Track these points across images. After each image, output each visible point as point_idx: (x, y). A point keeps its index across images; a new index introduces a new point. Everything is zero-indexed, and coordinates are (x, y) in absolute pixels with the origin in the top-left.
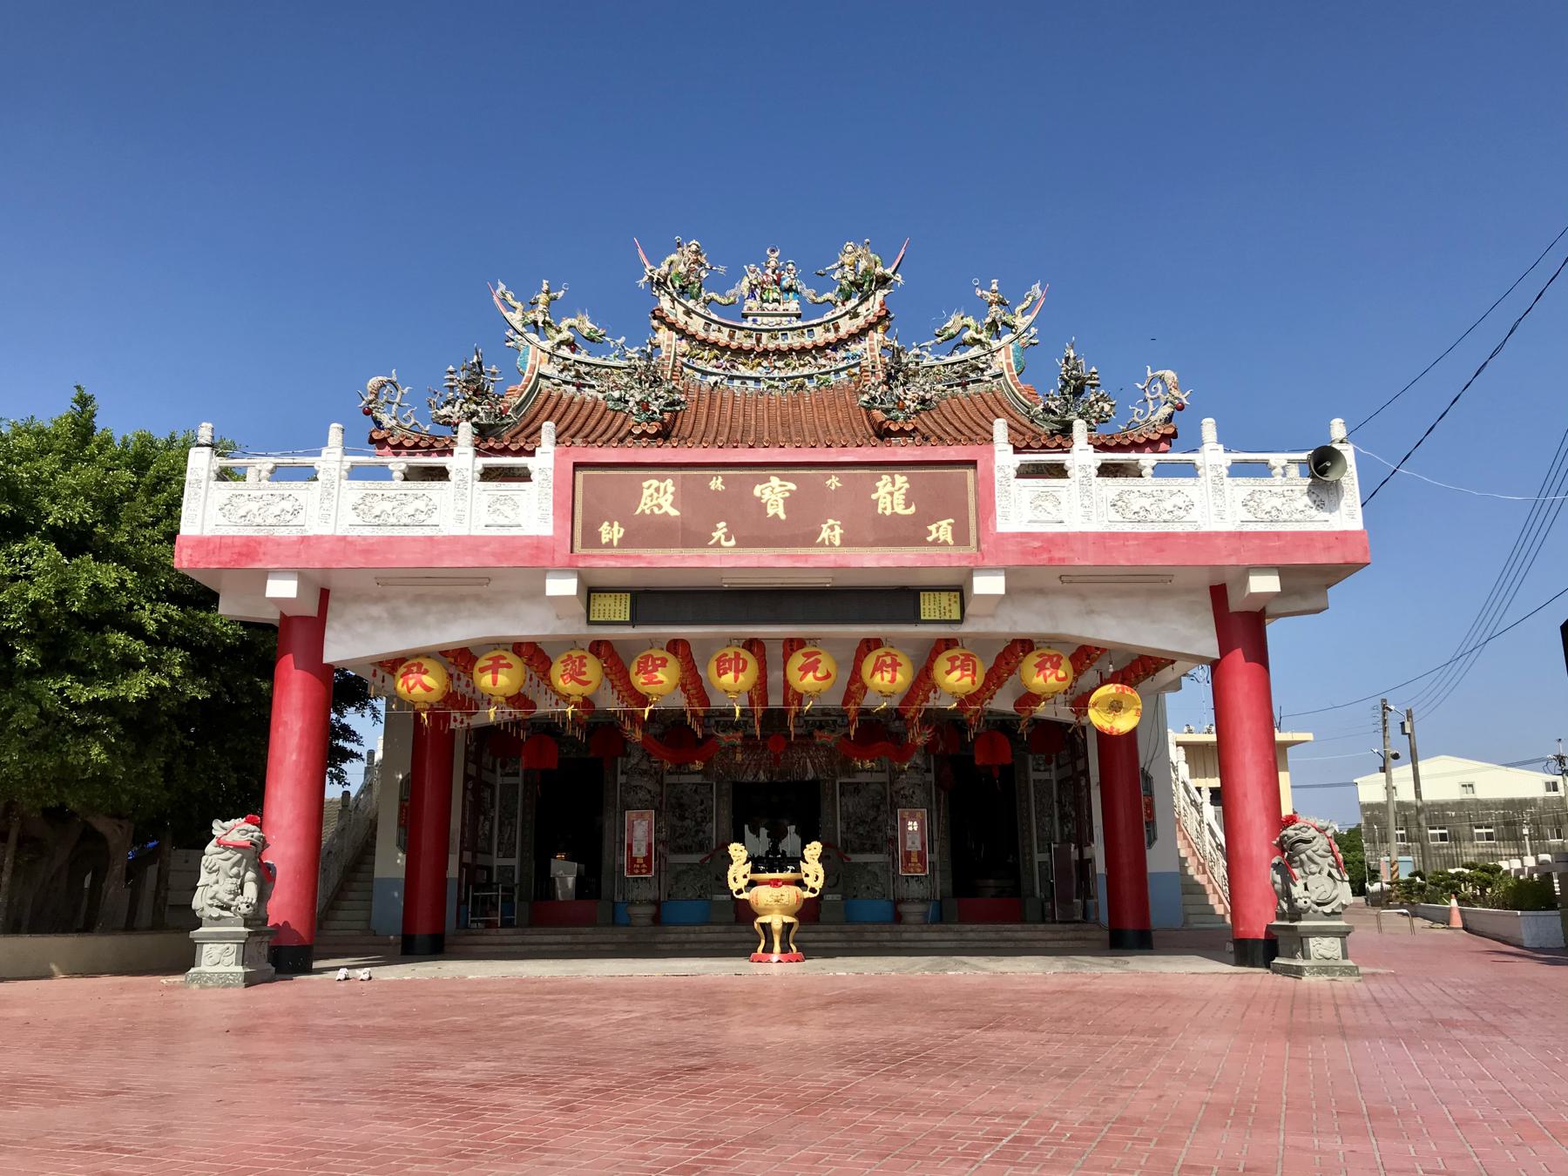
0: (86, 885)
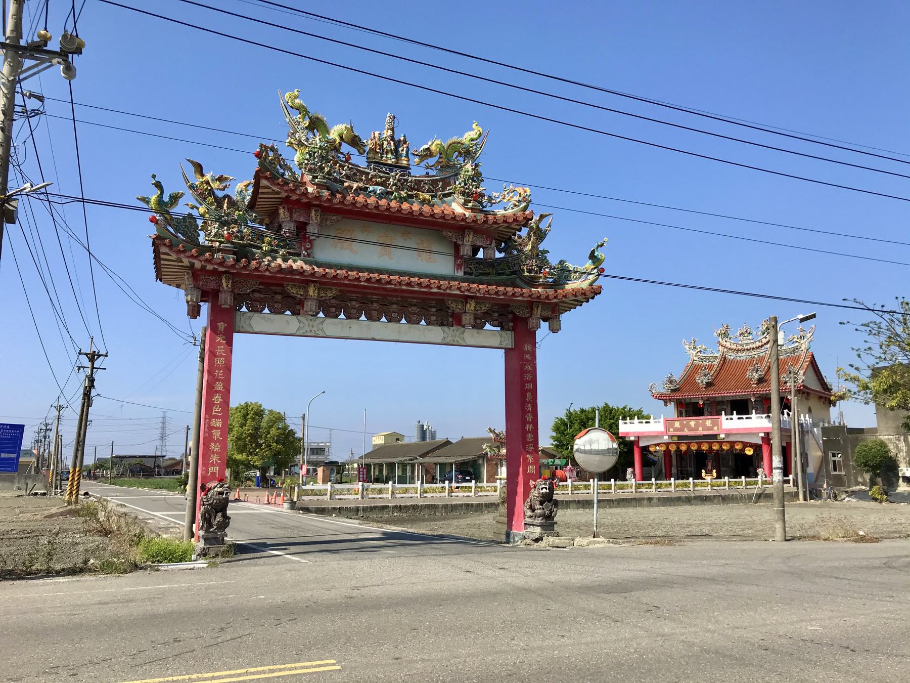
0: (329, 665)
